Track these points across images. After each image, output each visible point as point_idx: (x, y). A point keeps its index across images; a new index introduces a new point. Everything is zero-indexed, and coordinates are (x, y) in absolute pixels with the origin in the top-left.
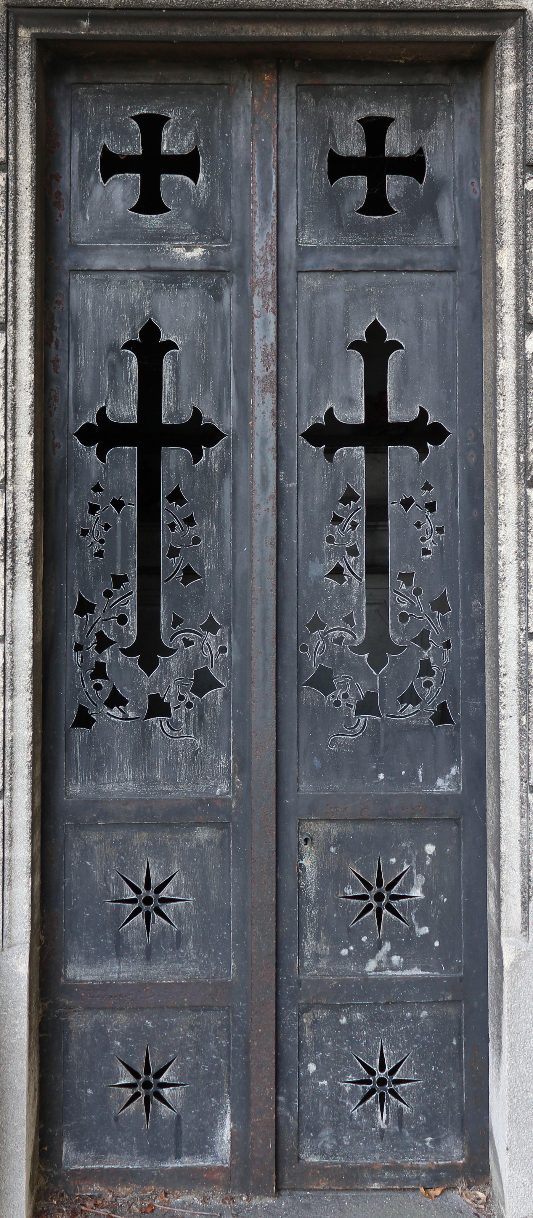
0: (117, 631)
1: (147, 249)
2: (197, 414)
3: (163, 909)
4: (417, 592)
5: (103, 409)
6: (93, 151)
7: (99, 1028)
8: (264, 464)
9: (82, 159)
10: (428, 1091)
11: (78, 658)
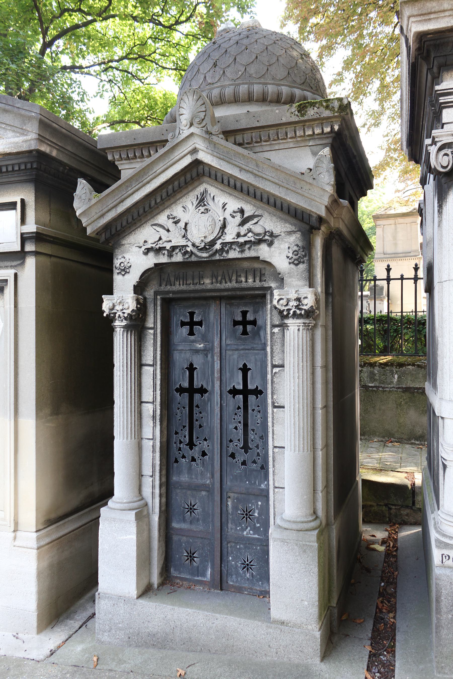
0: (184, 439)
1: (190, 344)
2: (202, 386)
3: (194, 511)
4: (256, 434)
5: (180, 384)
6: (178, 321)
7: (180, 540)
8: (217, 399)
9: (176, 323)
10: (260, 569)
11: (175, 445)
